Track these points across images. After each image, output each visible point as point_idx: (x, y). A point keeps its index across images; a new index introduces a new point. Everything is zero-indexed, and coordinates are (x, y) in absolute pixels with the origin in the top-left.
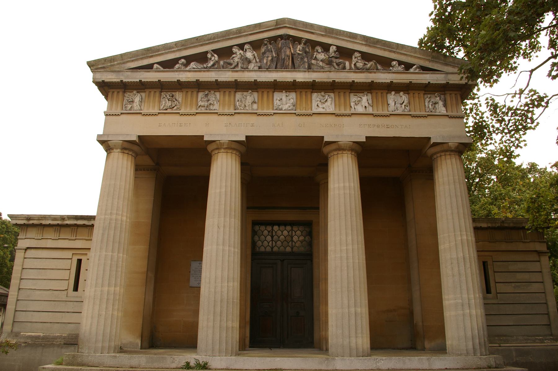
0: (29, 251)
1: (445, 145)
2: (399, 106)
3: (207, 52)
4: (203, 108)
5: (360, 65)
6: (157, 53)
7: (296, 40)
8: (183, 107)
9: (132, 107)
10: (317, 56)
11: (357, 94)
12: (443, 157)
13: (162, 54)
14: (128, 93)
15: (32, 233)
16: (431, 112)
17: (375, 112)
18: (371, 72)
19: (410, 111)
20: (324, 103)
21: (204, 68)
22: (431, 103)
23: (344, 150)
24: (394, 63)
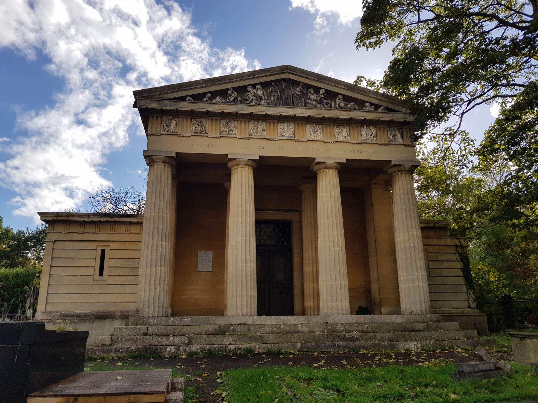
0: (57, 243)
1: (402, 167)
2: (369, 136)
3: (228, 89)
4: (225, 133)
5: (342, 105)
6: (189, 88)
7: (296, 83)
8: (210, 131)
9: (169, 130)
10: (311, 96)
11: (339, 126)
12: (400, 175)
13: (193, 89)
14: (165, 118)
15: (59, 228)
16: (392, 141)
17: (352, 141)
18: (350, 111)
19: (377, 141)
20: (315, 133)
21: (227, 102)
22: (392, 135)
23: (330, 168)
24: (367, 104)
